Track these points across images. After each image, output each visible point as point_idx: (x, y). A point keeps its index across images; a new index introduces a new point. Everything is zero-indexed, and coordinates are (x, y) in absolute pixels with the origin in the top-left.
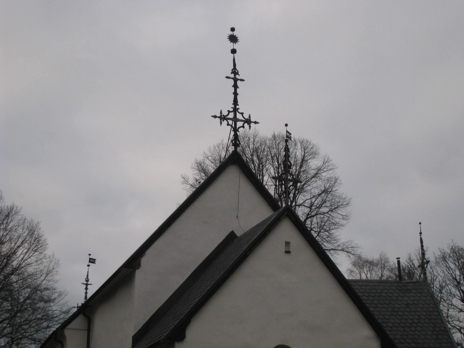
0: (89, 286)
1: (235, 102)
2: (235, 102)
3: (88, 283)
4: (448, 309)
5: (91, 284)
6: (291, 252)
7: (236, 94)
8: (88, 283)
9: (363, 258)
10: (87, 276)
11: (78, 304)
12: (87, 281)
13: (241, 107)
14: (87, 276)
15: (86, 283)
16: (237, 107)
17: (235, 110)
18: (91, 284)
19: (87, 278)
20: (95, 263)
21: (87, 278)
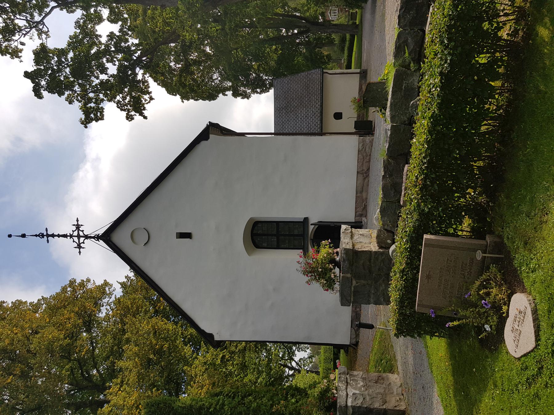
0: (50, 233)
1: (65, 236)
2: (65, 236)
3: (45, 234)
4: (532, 272)
5: (47, 229)
6: (307, 218)
7: (59, 236)
8: (45, 234)
9: (535, 32)
10: (36, 236)
11: (76, 247)
12: (42, 236)
13: (68, 232)
14: (36, 236)
15: (45, 237)
16: (68, 234)
17: (71, 236)
18: (47, 229)
19: (39, 236)
20: (105, 281)
21: (39, 236)
